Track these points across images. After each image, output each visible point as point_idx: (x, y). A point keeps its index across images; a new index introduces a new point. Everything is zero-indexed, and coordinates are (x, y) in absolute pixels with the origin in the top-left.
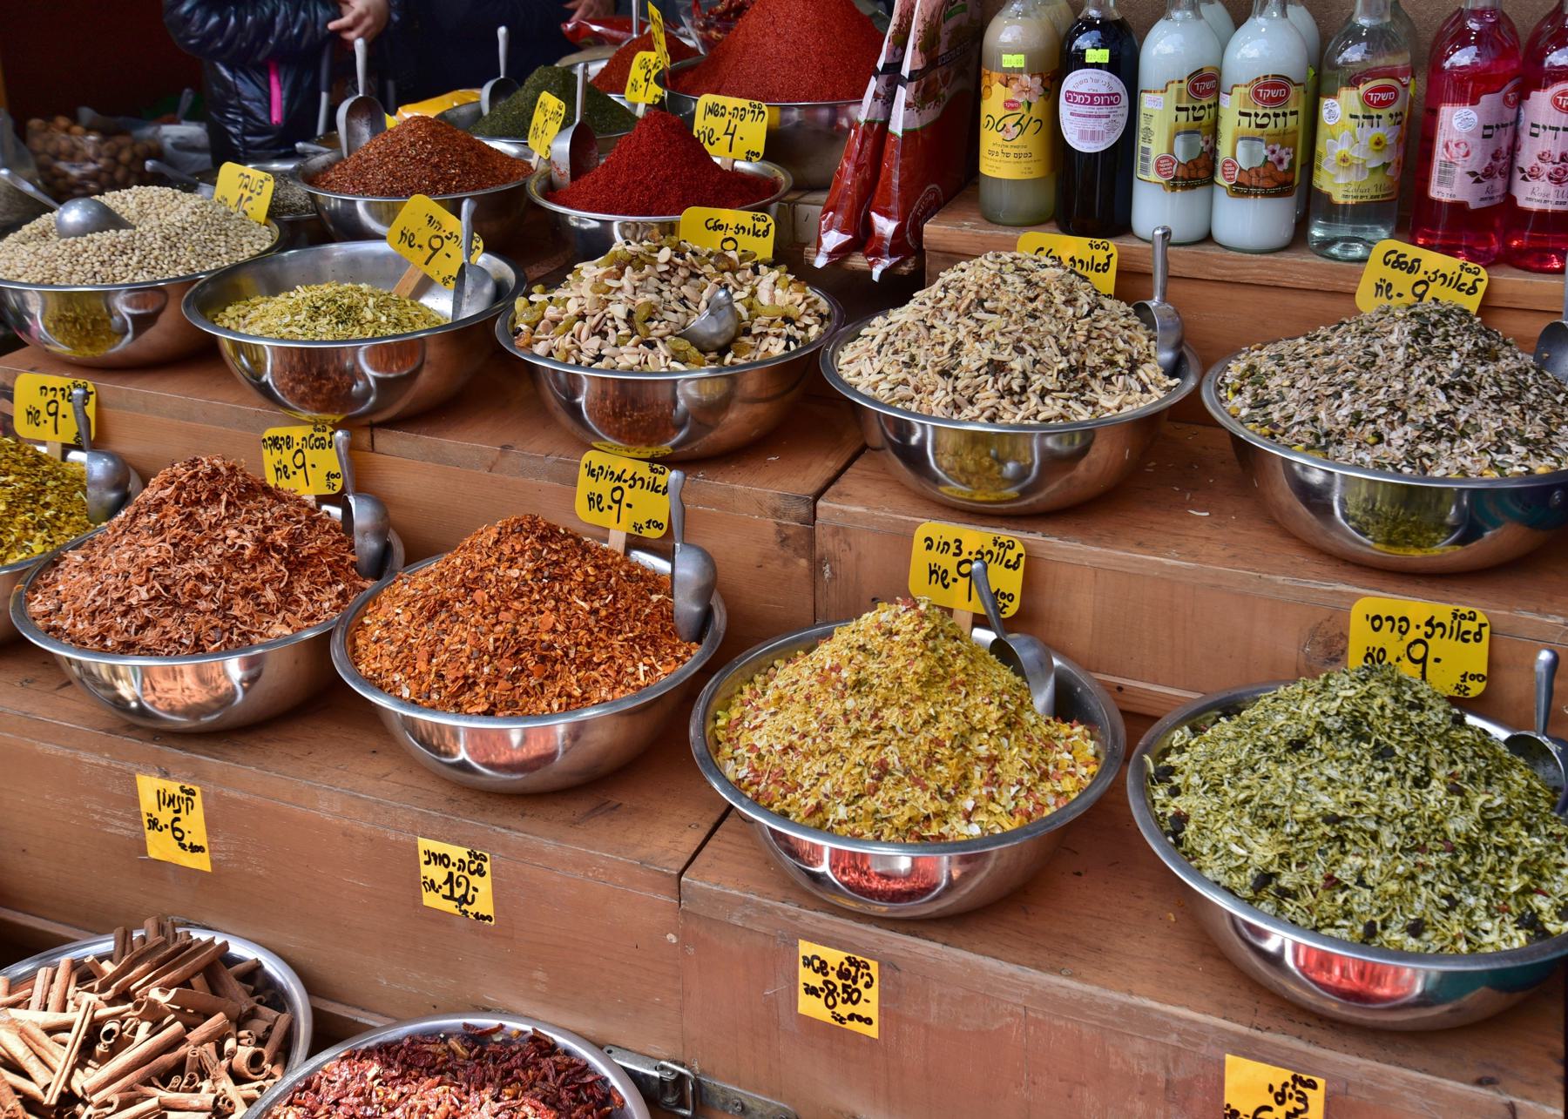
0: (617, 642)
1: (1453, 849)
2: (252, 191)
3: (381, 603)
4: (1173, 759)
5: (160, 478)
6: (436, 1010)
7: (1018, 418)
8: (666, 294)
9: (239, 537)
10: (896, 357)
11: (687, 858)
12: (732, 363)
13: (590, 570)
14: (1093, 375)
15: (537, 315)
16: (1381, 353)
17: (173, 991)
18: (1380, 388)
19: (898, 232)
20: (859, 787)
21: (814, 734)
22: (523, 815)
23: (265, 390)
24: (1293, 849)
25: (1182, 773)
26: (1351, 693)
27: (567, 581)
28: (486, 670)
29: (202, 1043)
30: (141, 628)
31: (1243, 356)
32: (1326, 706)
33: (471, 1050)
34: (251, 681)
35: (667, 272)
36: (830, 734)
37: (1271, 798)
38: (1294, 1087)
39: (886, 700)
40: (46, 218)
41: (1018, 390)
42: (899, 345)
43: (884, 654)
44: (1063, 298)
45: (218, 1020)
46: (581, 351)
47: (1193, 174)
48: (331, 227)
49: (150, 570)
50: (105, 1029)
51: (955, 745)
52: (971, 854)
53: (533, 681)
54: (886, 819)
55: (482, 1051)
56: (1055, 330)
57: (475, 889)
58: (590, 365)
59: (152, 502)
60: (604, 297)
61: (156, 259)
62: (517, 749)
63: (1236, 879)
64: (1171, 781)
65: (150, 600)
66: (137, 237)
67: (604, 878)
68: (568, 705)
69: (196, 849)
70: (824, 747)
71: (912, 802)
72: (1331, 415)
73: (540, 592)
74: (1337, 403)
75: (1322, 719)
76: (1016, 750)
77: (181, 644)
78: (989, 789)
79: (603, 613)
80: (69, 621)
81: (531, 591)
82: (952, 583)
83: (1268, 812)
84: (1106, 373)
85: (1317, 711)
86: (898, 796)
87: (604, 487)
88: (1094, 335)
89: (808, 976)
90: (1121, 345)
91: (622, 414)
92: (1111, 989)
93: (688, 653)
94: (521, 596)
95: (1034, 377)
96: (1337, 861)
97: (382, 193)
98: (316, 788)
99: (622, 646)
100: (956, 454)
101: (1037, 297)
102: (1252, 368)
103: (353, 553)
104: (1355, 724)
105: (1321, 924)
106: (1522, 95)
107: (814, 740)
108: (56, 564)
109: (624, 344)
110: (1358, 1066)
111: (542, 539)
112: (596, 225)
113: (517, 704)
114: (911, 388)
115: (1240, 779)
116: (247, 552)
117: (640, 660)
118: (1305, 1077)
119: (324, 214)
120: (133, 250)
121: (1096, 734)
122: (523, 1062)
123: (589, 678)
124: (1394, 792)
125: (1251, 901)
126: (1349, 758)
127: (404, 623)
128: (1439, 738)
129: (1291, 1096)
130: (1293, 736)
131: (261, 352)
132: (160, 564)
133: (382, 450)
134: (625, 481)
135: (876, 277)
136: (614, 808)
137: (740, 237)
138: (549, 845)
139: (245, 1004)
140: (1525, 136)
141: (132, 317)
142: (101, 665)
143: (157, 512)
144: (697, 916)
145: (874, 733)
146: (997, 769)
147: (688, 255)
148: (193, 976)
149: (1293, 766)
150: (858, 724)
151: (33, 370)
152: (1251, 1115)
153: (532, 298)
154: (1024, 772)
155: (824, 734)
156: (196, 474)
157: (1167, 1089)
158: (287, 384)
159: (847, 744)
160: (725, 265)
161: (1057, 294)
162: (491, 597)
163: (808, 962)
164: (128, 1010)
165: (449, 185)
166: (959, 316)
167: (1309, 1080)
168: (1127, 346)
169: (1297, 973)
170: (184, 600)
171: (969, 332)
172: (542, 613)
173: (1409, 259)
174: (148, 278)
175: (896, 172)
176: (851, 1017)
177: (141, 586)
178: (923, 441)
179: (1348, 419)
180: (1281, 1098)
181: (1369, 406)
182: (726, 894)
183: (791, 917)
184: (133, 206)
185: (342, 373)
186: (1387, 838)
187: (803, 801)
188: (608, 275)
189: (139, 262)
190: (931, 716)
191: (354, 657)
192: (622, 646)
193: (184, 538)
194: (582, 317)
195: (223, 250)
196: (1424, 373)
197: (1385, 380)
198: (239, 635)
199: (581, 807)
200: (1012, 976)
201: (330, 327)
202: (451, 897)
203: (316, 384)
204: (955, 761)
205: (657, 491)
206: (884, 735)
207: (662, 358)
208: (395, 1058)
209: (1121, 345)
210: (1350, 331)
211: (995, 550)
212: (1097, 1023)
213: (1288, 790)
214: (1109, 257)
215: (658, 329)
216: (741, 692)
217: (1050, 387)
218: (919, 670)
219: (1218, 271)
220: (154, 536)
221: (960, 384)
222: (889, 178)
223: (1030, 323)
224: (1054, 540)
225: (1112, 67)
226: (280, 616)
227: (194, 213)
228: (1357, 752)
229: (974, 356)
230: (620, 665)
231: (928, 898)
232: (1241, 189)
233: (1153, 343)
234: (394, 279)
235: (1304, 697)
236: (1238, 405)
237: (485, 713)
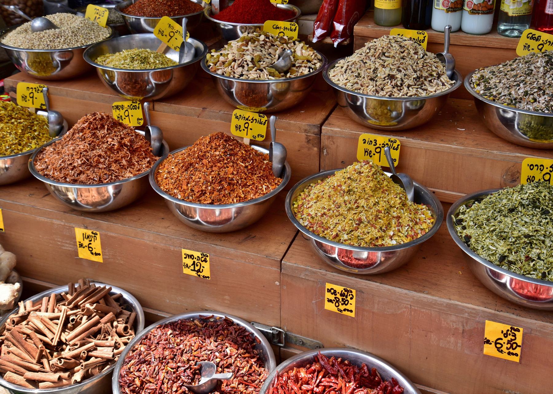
0: (255, 177)
2: (100, 15)
3: (165, 165)
4: (461, 216)
5: (82, 120)
6: (187, 311)
7: (400, 95)
8: (264, 52)
9: (112, 141)
10: (352, 74)
11: (283, 255)
12: (289, 77)
13: (244, 152)
14: (425, 80)
15: (217, 60)
16: (534, 69)
17: (95, 305)
18: (534, 82)
19: (344, 29)
20: (351, 228)
21: (333, 209)
22: (221, 240)
23: (114, 87)
24: (512, 247)
25: (466, 221)
26: (533, 191)
27: (236, 156)
28: (209, 188)
29: (106, 323)
30: (79, 174)
31: (476, 72)
32: (523, 196)
33: (202, 324)
34: (116, 194)
35: (263, 44)
36: (339, 209)
37: (504, 229)
38: (511, 331)
39: (360, 197)
40: (26, 25)
41: (400, 85)
42: (353, 69)
43: (358, 180)
44: (414, 52)
45: (110, 315)
46: (234, 73)
47: (456, 6)
48: (130, 28)
49: (81, 153)
50: (70, 319)
51: (385, 212)
52: (390, 252)
53: (227, 192)
54: (362, 239)
55: (206, 325)
56: (411, 63)
57: (203, 267)
58: (239, 78)
59: (80, 129)
60: (242, 53)
61: (70, 40)
62: (218, 216)
63: (492, 258)
64: (462, 224)
65: (82, 164)
66: (62, 31)
67: (252, 262)
68: (240, 200)
69: (97, 254)
70: (337, 214)
71: (371, 233)
72: (516, 92)
73: (227, 160)
74: (518, 88)
75: (521, 201)
76: (406, 214)
77: (94, 180)
78: (398, 228)
79: (249, 167)
80: (52, 172)
81: (224, 160)
82: (373, 156)
83: (502, 234)
84: (430, 79)
85: (519, 198)
86: (366, 231)
87: (242, 122)
88: (425, 65)
90: (434, 69)
91: (249, 95)
92: (443, 298)
93: (278, 181)
94: (220, 161)
95: (405, 80)
96: (530, 251)
97: (150, 16)
98: (143, 231)
99: (257, 179)
100: (374, 108)
101: (404, 51)
102: (482, 76)
103: (151, 147)
105: (525, 273)
107: (333, 211)
108: (42, 152)
109: (251, 70)
110: (536, 323)
111: (226, 141)
112: (231, 27)
113: (221, 200)
114: (359, 85)
115: (490, 223)
116: (116, 147)
117: (263, 184)
118: (515, 328)
119: (127, 23)
120: (61, 36)
121: (430, 209)
122: (223, 328)
123: (246, 191)
125: (498, 265)
126: (532, 214)
127: (176, 172)
129: (510, 334)
130: (510, 206)
131: (113, 74)
132: (85, 151)
133: (157, 110)
134: (249, 120)
135: (335, 46)
136: (253, 237)
137: (285, 32)
138: (232, 251)
139: (119, 309)
141: (60, 61)
142: (63, 186)
143: (82, 132)
144: (288, 275)
145: (356, 208)
146: (400, 221)
147: (270, 38)
148: (100, 299)
149: (510, 217)
150: (350, 205)
151: (23, 81)
152: (494, 341)
153: (212, 54)
154: (409, 222)
155: (337, 209)
156: (96, 118)
157: (463, 333)
158: (123, 85)
159: (346, 213)
160: (283, 41)
161: (411, 50)
162: (209, 162)
163: (329, 291)
164: (80, 311)
165: (175, 13)
166: (375, 59)
167: (517, 329)
168: (436, 69)
169: (511, 290)
170: (94, 164)
171: (380, 65)
172: (228, 167)
173: (536, 36)
174: (68, 47)
175: (344, 7)
176: (345, 310)
177: (78, 159)
178: (362, 103)
179: (523, 94)
180: (506, 335)
181: (531, 89)
182: (299, 267)
183: (323, 275)
184: (58, 20)
185: (144, 81)
187: (331, 233)
188: (243, 45)
189: (64, 41)
190: (376, 202)
191: (159, 185)
192: (257, 179)
193: (93, 142)
194: (234, 60)
195: (93, 37)
196: (551, 77)
197: (536, 79)
198: (115, 177)
199: (242, 237)
200: (406, 294)
201: (138, 65)
202: (194, 270)
203: (134, 86)
204: (386, 218)
205: (262, 124)
206: (360, 209)
207: (266, 75)
208: (176, 327)
209: (434, 69)
210: (520, 62)
211: (389, 143)
212: (438, 310)
213: (510, 226)
214: (424, 37)
215: (263, 65)
216: (300, 195)
217: (411, 84)
218: (371, 186)
219: (464, 42)
220: (82, 141)
221: (378, 83)
222: (341, 9)
223: (402, 61)
224: (411, 139)
226: (128, 170)
227: (82, 23)
228: (535, 212)
229: (382, 73)
230: (257, 186)
231: (372, 267)
232: (474, 12)
233: (444, 68)
234: (156, 48)
235: (513, 193)
236: (479, 90)
237: (210, 203)
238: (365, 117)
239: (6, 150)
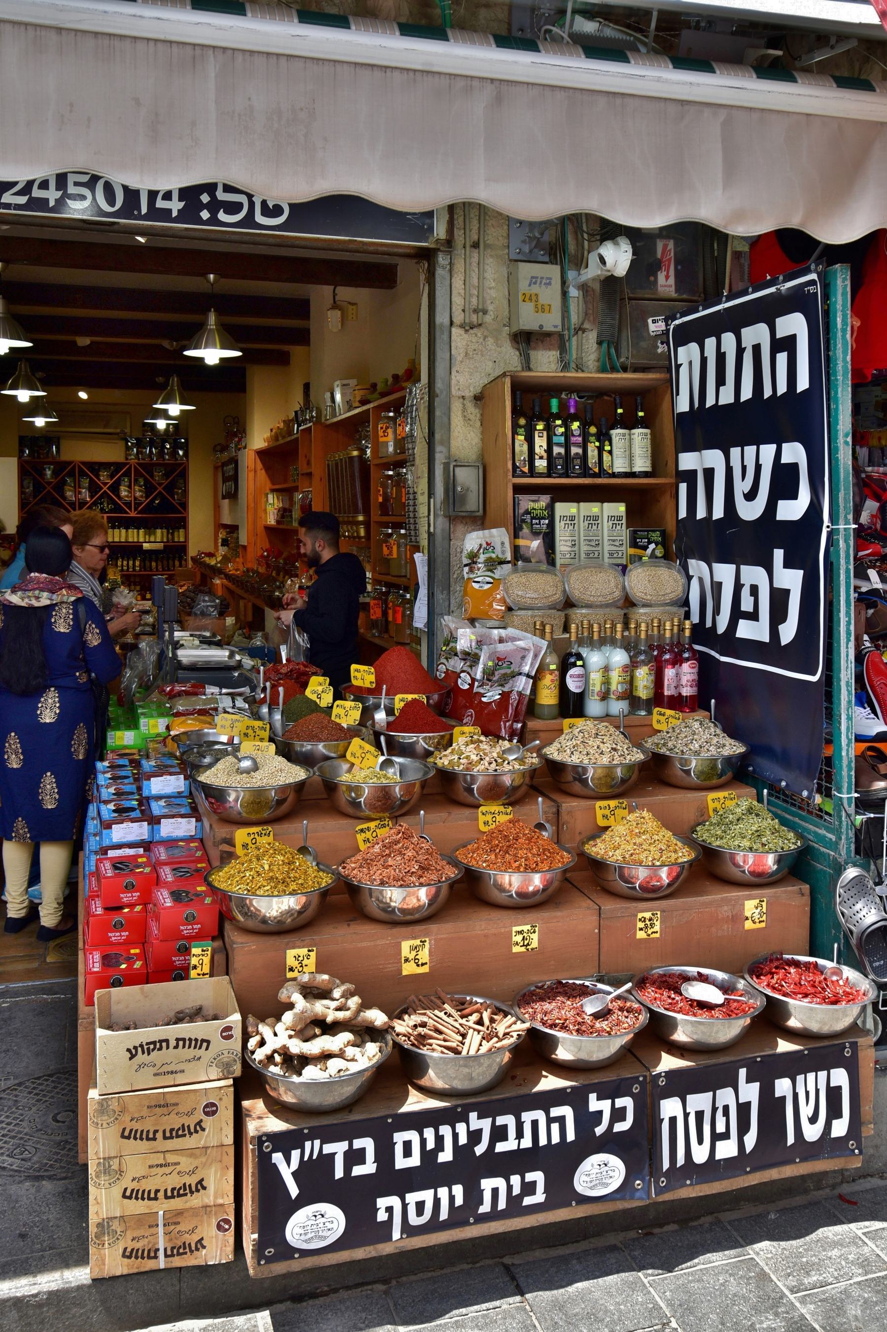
69: (423, 964)
89: (640, 925)
163: (640, 920)
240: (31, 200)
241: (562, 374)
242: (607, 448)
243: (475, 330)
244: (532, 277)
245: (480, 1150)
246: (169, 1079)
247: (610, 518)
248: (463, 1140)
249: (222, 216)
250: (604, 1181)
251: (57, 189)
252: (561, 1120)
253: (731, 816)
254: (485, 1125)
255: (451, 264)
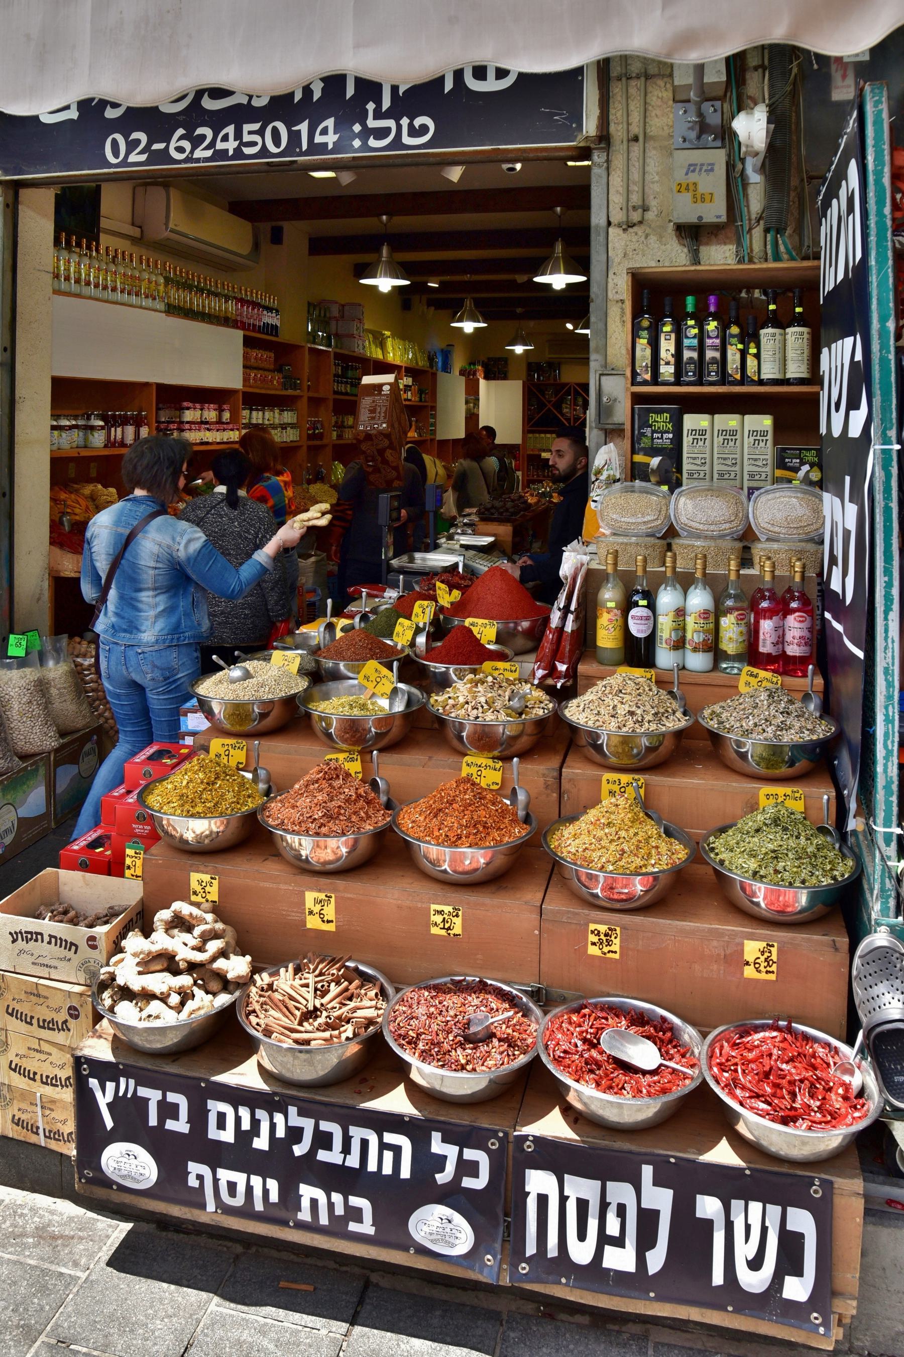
0: (506, 821)
1: (810, 857)
19: (567, 669)
30: (319, 827)
69: (328, 922)
72: (747, 725)
89: (593, 938)
91: (482, 739)
102: (713, 712)
104: (775, 821)
106: (785, 617)
112: (444, 669)
124: (790, 841)
128: (800, 823)
140: (787, 631)
163: (592, 932)
176: (609, 952)
180: (763, 953)
185: (364, 730)
186: (791, 855)
188: (472, 687)
194: (467, 703)
202: (444, 928)
206: (622, 840)
221: (620, 720)
222: (564, 648)
225: (647, 607)
232: (695, 650)
238: (604, 755)
239: (227, 809)
240: (217, 152)
241: (693, 268)
242: (753, 351)
243: (635, 229)
244: (690, 165)
245: (299, 1150)
246: (44, 972)
247: (752, 433)
248: (281, 1133)
249: (373, 143)
250: (447, 1238)
251: (235, 140)
252: (397, 1150)
253: (750, 824)
254: (308, 1124)
255: (608, 161)
